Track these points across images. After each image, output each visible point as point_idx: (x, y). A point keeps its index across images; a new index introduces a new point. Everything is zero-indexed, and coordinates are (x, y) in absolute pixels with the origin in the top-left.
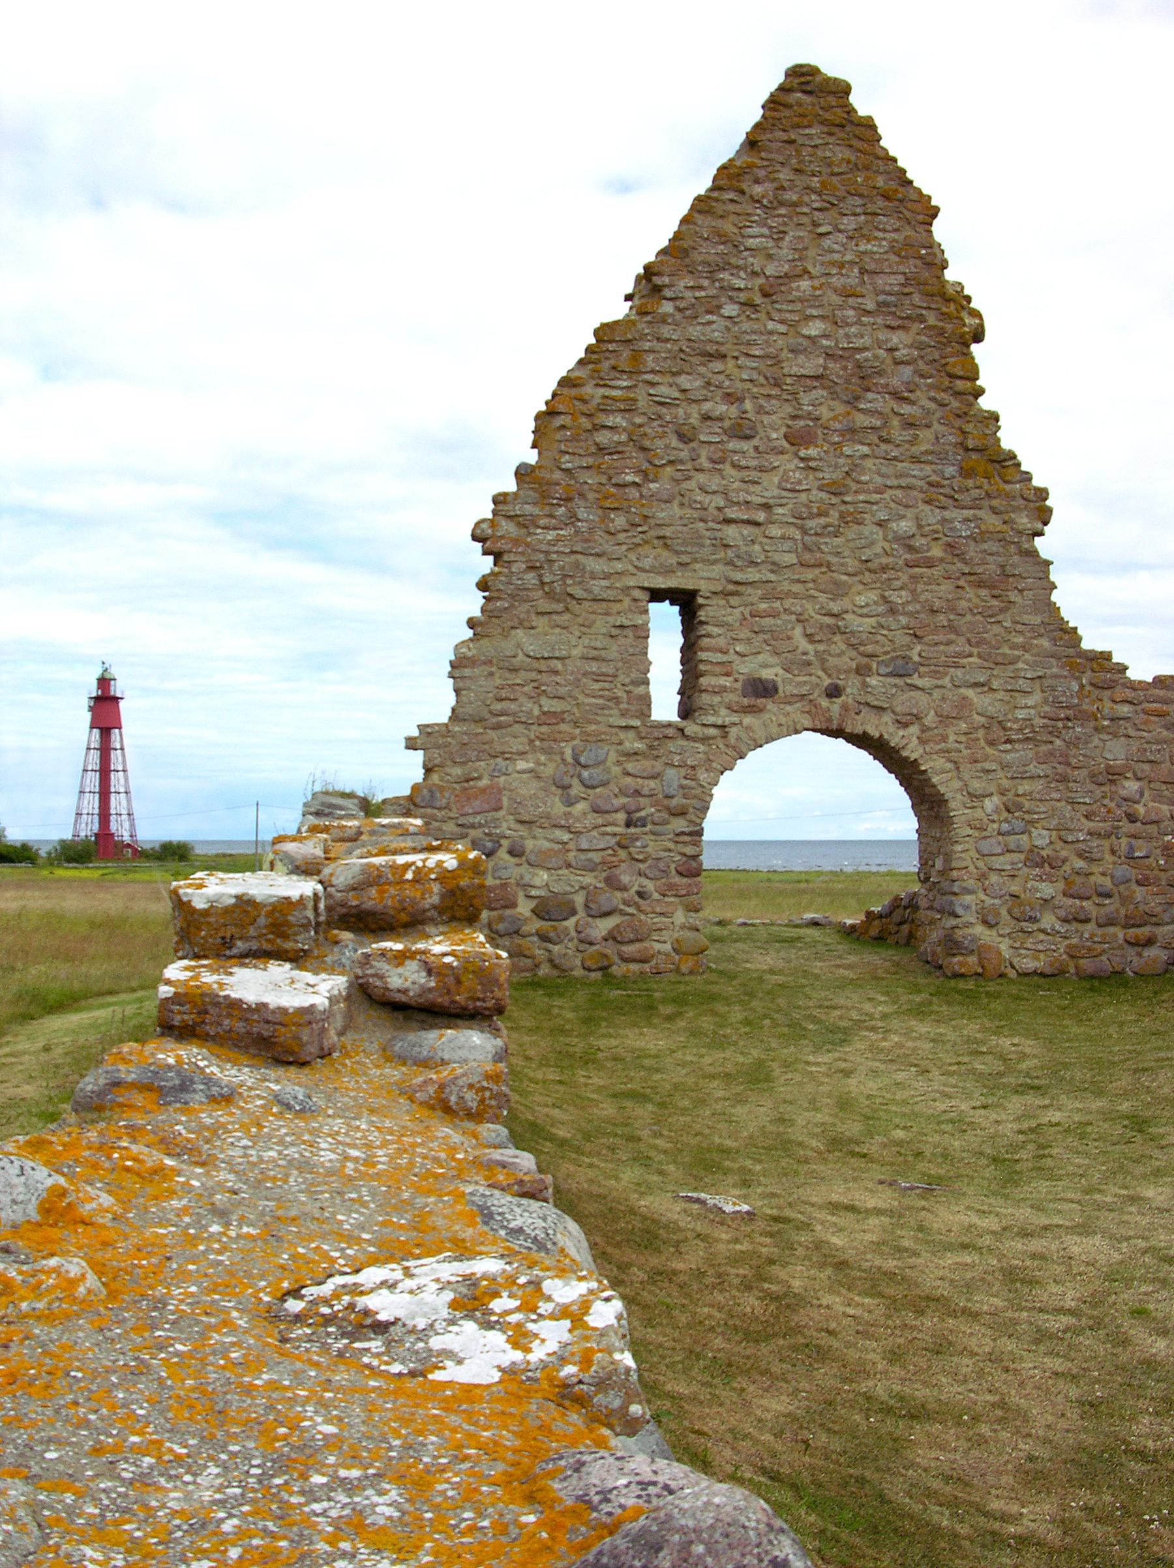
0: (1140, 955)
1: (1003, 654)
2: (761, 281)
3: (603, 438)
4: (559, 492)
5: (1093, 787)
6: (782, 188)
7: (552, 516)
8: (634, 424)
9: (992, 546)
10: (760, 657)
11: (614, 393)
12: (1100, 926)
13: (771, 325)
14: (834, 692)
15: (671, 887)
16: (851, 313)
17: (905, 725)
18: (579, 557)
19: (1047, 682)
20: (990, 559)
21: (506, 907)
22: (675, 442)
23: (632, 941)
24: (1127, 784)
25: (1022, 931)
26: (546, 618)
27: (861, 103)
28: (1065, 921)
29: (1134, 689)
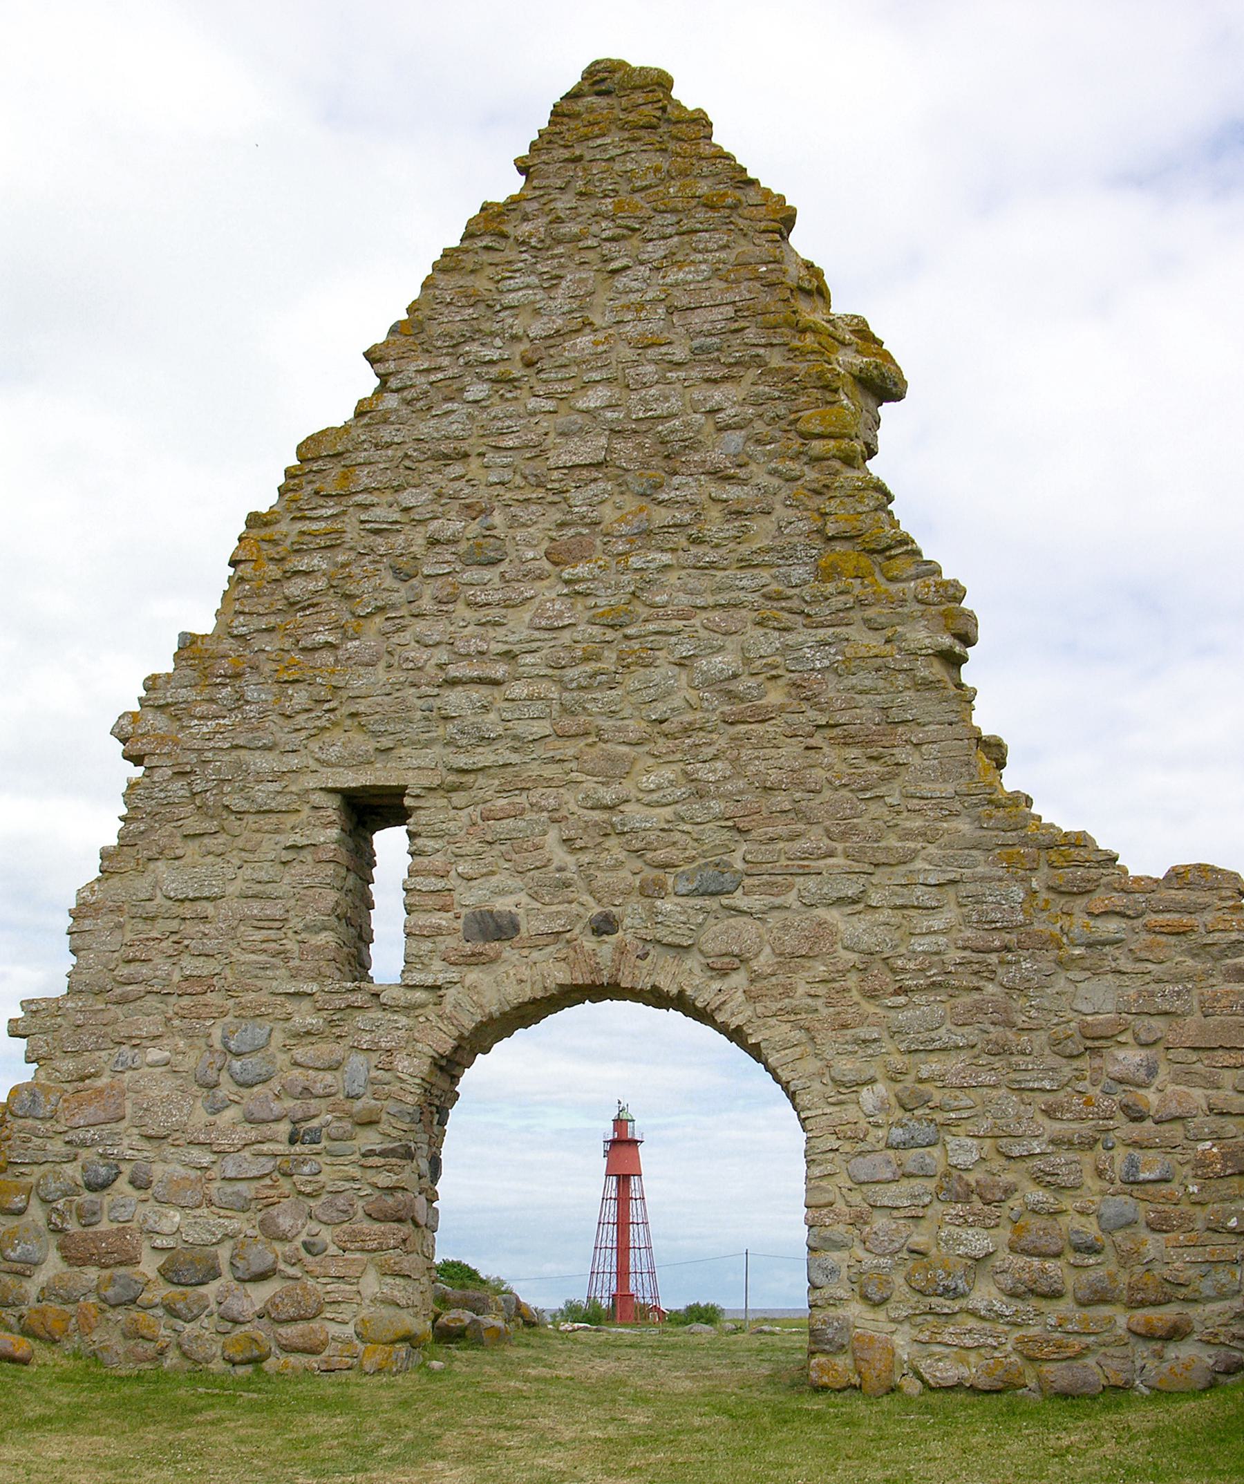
0: (1160, 1357)
1: (887, 849)
2: (524, 346)
3: (295, 588)
4: (224, 666)
5: (1053, 1061)
6: (559, 220)
7: (212, 701)
8: (336, 564)
9: (865, 680)
10: (494, 880)
11: (314, 526)
12: (1082, 1304)
13: (533, 403)
14: (604, 926)
15: (354, 1236)
16: (651, 368)
17: (723, 973)
18: (243, 752)
19: (964, 890)
20: (864, 699)
21: (121, 1263)
22: (389, 581)
23: (293, 1320)
24: (1121, 1054)
25: (931, 1311)
26: (197, 842)
27: (686, 95)
28: (1013, 1295)
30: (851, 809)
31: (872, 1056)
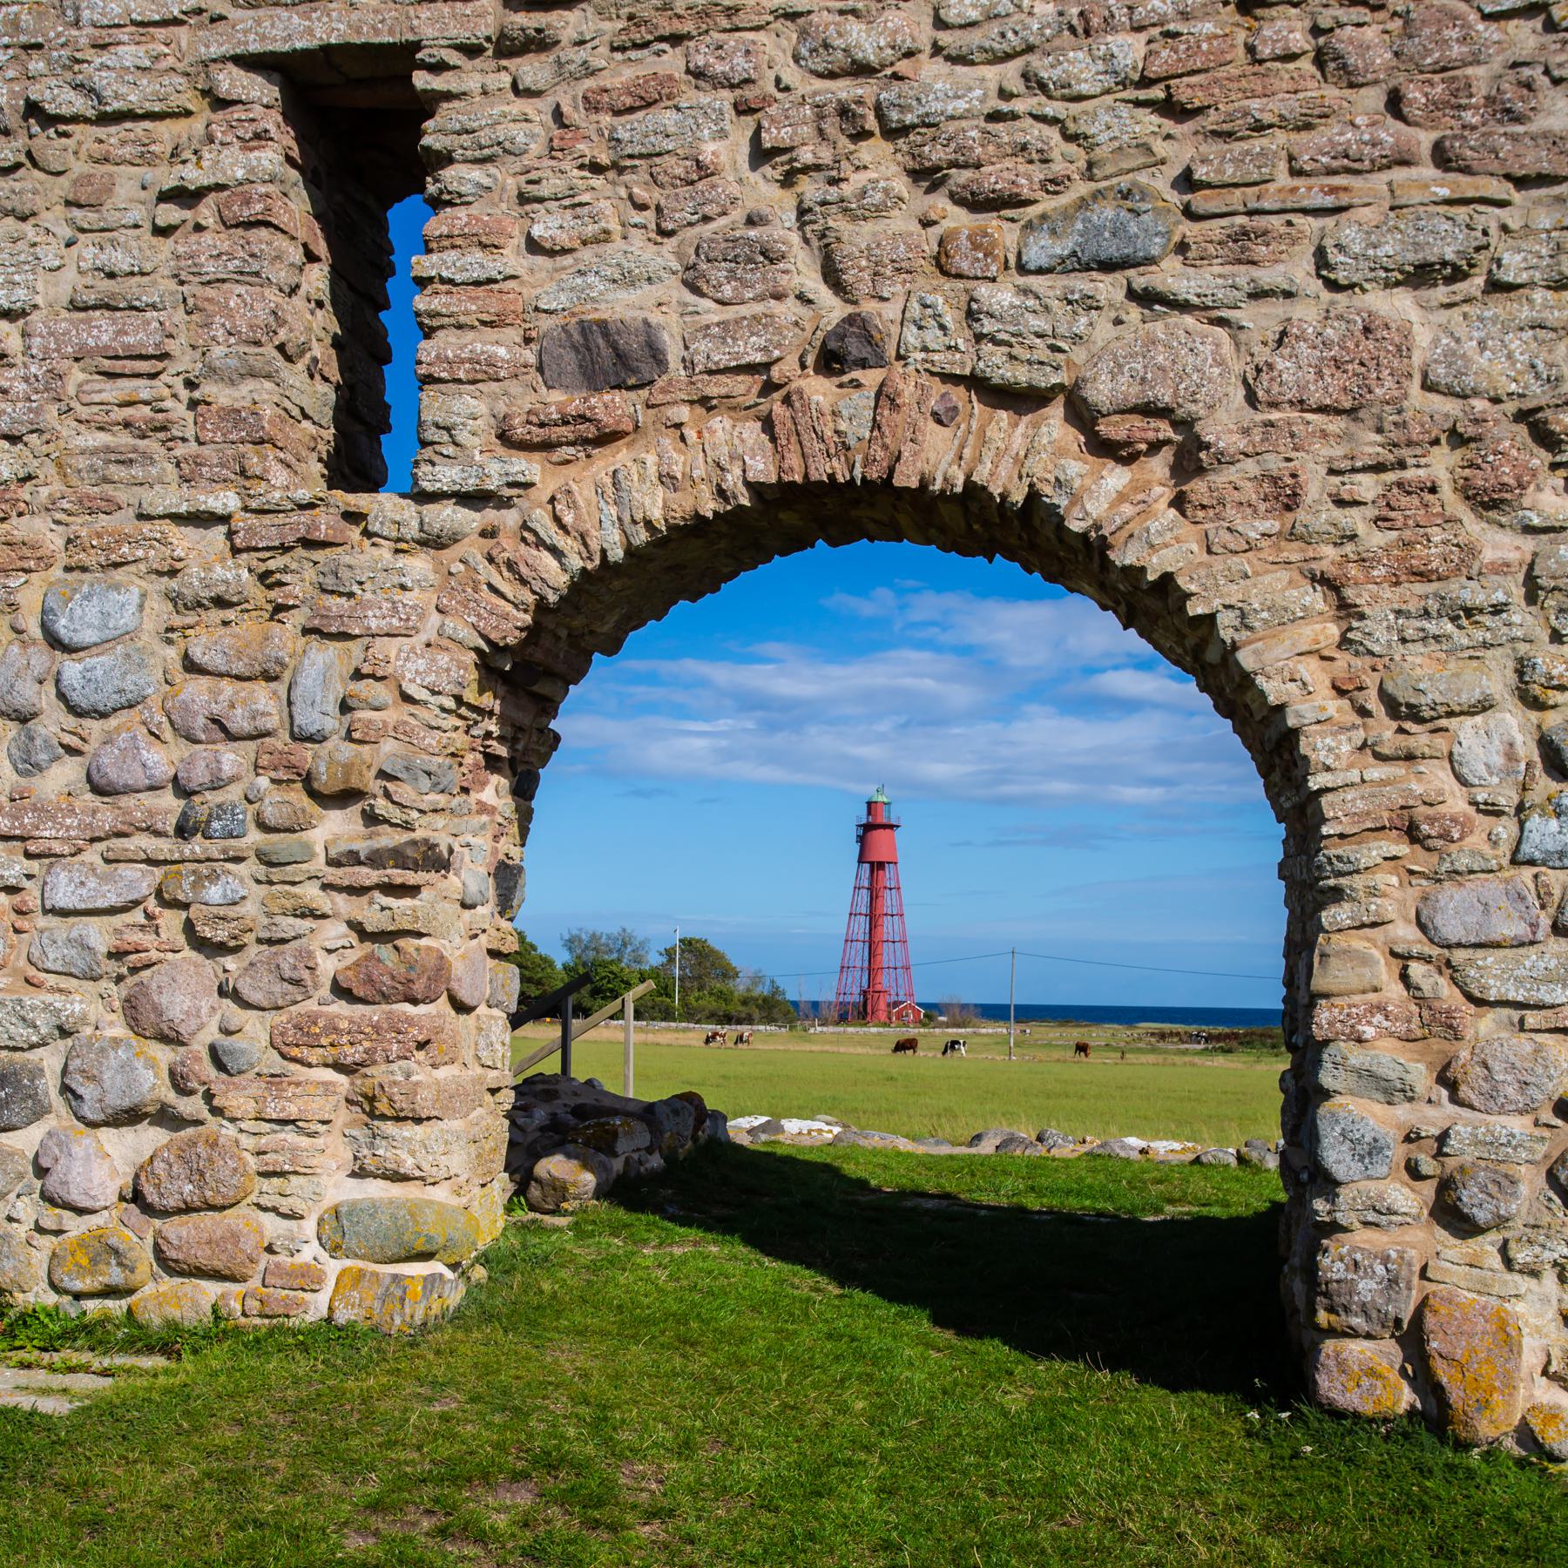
15: (306, 1031)
23: (188, 1209)
29: (167, 1349)
30: (1463, 40)
31: (1486, 645)
